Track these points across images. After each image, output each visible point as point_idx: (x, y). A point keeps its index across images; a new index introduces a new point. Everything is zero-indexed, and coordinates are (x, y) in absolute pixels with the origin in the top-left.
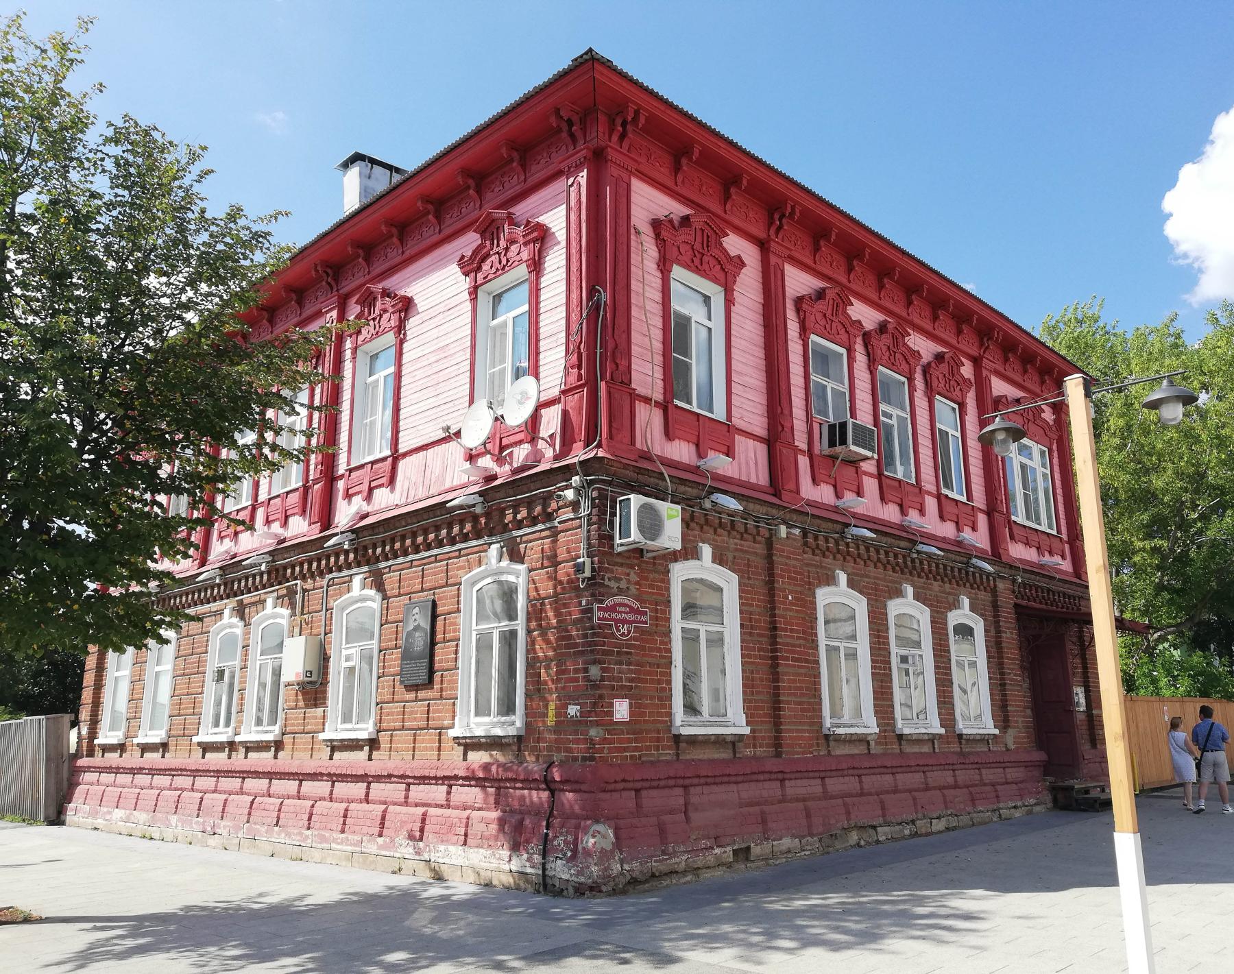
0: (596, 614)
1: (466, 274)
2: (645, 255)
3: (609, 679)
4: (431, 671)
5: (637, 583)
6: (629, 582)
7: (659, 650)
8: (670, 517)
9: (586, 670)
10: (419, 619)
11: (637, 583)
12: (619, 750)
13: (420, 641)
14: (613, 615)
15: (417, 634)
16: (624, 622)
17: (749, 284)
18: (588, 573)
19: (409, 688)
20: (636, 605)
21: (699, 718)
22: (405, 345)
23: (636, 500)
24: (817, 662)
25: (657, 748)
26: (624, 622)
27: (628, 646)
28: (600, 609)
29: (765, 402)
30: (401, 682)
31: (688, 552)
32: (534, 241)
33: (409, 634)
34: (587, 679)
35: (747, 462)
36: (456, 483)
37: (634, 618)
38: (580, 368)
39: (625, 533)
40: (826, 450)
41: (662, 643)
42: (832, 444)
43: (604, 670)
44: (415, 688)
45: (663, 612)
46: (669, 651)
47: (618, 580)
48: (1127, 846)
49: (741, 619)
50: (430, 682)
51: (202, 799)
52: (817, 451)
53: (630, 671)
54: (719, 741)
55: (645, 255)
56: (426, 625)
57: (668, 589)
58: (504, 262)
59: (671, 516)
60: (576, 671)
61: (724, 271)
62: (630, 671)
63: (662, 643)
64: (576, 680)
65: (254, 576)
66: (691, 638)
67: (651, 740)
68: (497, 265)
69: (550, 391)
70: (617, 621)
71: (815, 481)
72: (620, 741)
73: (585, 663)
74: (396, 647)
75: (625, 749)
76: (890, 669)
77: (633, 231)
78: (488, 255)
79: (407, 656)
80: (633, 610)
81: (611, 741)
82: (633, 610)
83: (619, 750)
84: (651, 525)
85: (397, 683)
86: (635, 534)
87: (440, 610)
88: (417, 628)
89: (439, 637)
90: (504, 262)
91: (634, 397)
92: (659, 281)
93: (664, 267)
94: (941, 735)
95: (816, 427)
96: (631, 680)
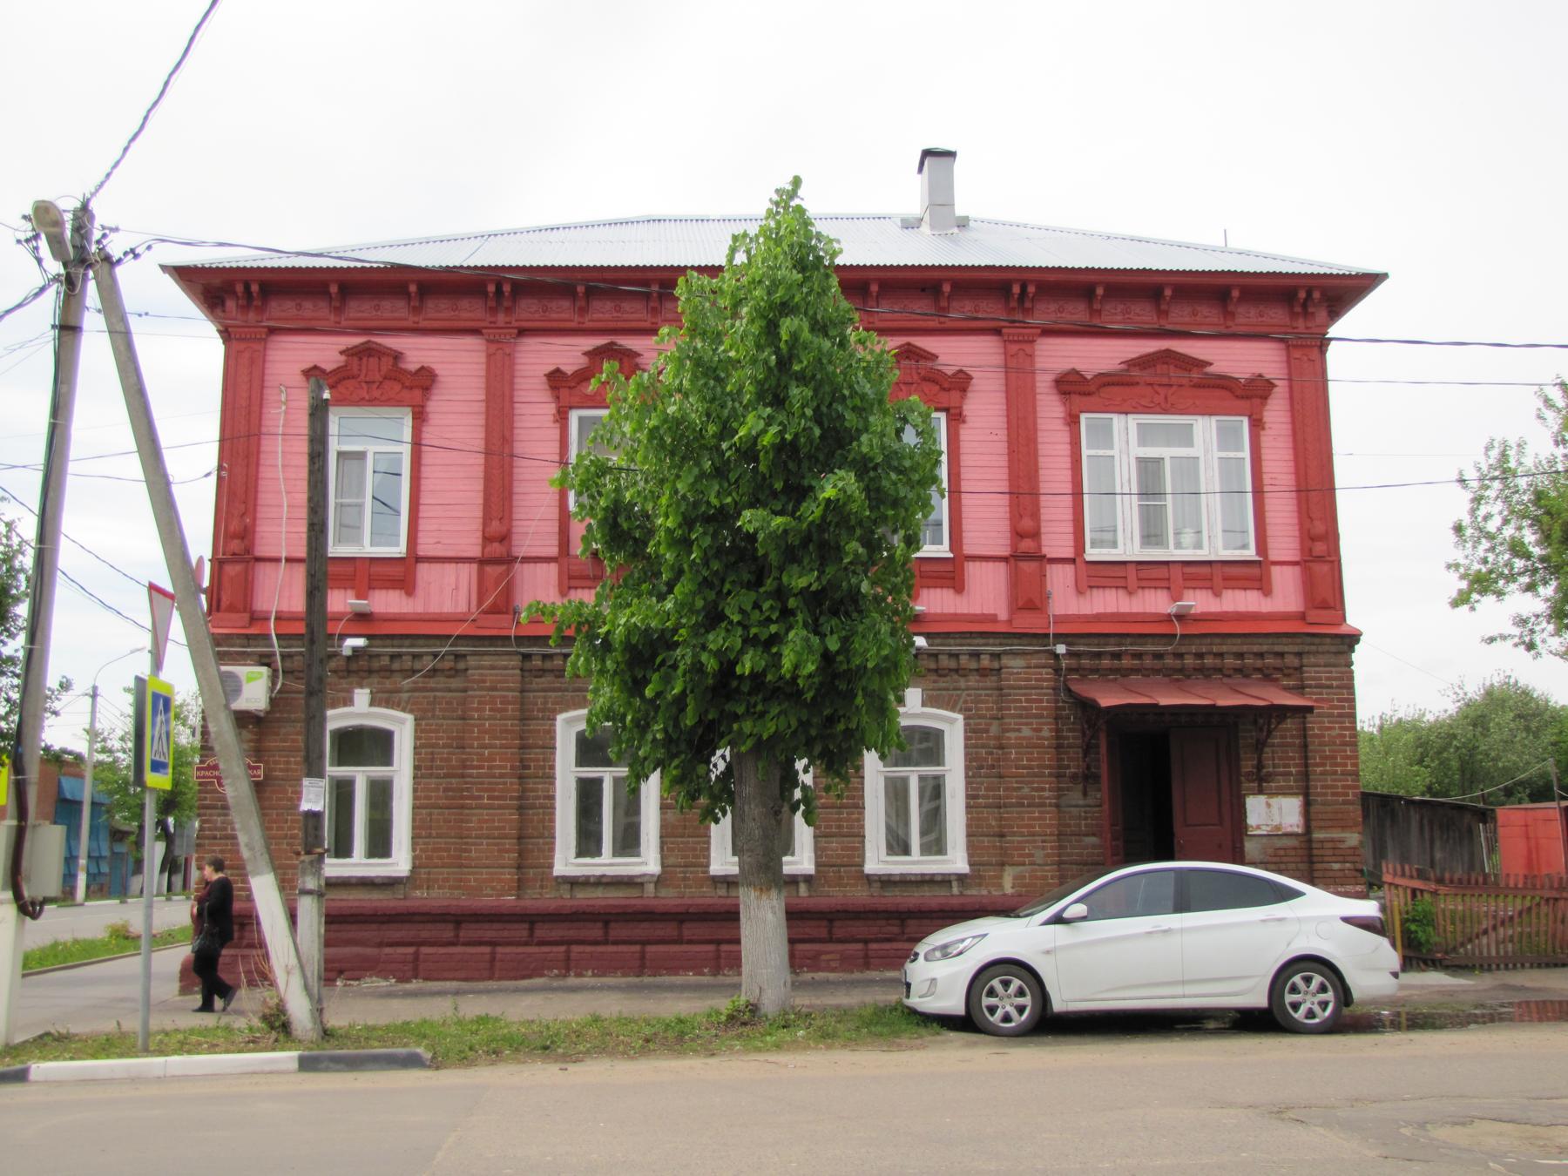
21: (597, 860)
61: (416, 389)
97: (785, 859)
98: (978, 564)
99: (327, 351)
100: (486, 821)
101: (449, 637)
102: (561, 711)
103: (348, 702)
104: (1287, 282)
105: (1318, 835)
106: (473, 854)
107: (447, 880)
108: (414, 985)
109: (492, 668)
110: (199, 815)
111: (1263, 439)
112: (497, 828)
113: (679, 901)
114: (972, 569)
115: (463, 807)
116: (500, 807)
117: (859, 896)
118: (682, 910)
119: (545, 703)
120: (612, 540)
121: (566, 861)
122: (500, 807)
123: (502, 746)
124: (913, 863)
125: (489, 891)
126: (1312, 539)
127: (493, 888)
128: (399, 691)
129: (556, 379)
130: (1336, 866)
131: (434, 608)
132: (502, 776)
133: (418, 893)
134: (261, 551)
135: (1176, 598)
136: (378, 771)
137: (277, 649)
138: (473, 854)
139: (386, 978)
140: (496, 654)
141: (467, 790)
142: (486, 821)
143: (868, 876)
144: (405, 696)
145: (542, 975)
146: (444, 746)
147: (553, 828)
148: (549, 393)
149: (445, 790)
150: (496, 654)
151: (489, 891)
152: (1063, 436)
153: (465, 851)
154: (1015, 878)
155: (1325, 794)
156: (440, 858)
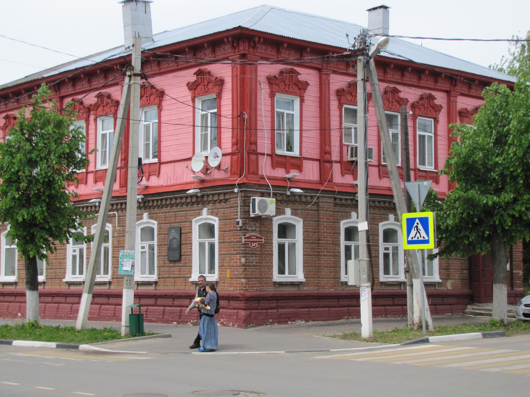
0: (243, 240)
1: (190, 89)
2: (264, 90)
3: (248, 262)
4: (181, 256)
5: (259, 227)
6: (256, 227)
7: (268, 251)
8: (271, 204)
9: (240, 259)
10: (174, 234)
11: (259, 227)
12: (252, 287)
13: (175, 244)
14: (250, 240)
15: (174, 241)
16: (254, 242)
17: (312, 93)
18: (240, 225)
19: (171, 261)
20: (259, 235)
21: (284, 275)
22: (162, 113)
23: (258, 199)
24: (340, 252)
25: (267, 286)
26: (254, 242)
27: (255, 251)
28: (245, 238)
29: (319, 142)
30: (168, 259)
31: (279, 212)
32: (219, 85)
33: (171, 240)
34: (240, 262)
35: (311, 172)
36: (189, 180)
37: (258, 240)
38: (237, 144)
39: (254, 211)
40: (349, 159)
41: (269, 248)
42: (352, 156)
43: (246, 259)
44: (175, 261)
45: (270, 237)
46: (272, 251)
47: (252, 227)
48: (8, 247)
49: (304, 237)
50: (180, 260)
51: (72, 307)
52: (345, 159)
53: (256, 259)
54: (292, 284)
55: (264, 90)
56: (177, 237)
57: (272, 228)
58: (207, 89)
59: (271, 203)
60: (237, 259)
61: (300, 88)
62: (256, 259)
63: (269, 248)
64: (237, 263)
65: (91, 207)
66: (281, 247)
67: (265, 283)
68: (203, 90)
69: (226, 150)
70: (251, 242)
71: (343, 175)
72: (253, 284)
73: (240, 257)
74: (165, 245)
75: (254, 287)
76: (378, 254)
77: (258, 83)
78: (199, 84)
79: (170, 249)
80: (257, 238)
81: (249, 284)
82: (257, 238)
83: (252, 287)
84: (263, 206)
85: (166, 260)
86: (257, 212)
87: (183, 231)
88: (174, 238)
89: (183, 242)
90: (207, 89)
91: (258, 154)
92: (270, 102)
93: (272, 95)
94: (439, 283)
95: (345, 149)
96: (257, 263)
97: (97, 276)
98: (307, 161)
99: (274, 69)
100: (326, 261)
101: (319, 190)
102: (342, 220)
103: (387, 219)
104: (325, 48)
105: (514, 271)
106: (323, 273)
107: (312, 283)
108: (310, 323)
109: (326, 202)
110: (245, 257)
111: (303, 106)
112: (328, 263)
113: (317, 292)
114: (306, 163)
115: (319, 255)
116: (329, 256)
117: (270, 290)
118: (378, 294)
119: (337, 217)
120: (465, 173)
121: (277, 277)
122: (329, 256)
123: (330, 233)
124: (101, 277)
125: (327, 287)
126: (251, 144)
127: (328, 286)
128: (297, 210)
129: (271, 80)
130: (518, 282)
131: (307, 178)
132: (330, 244)
133: (305, 288)
134: (259, 151)
135: (288, 172)
136: (395, 244)
137: (272, 191)
138: (323, 273)
139: (302, 321)
140: (328, 197)
141: (321, 249)
142: (326, 261)
143: (342, 282)
144: (300, 211)
145: (343, 318)
146: (312, 232)
147: (340, 264)
148: (336, 97)
149: (312, 249)
150: (328, 197)
151: (327, 287)
152: (269, 102)
153: (319, 272)
154: (452, 284)
155: (324, 252)
156: (311, 275)
